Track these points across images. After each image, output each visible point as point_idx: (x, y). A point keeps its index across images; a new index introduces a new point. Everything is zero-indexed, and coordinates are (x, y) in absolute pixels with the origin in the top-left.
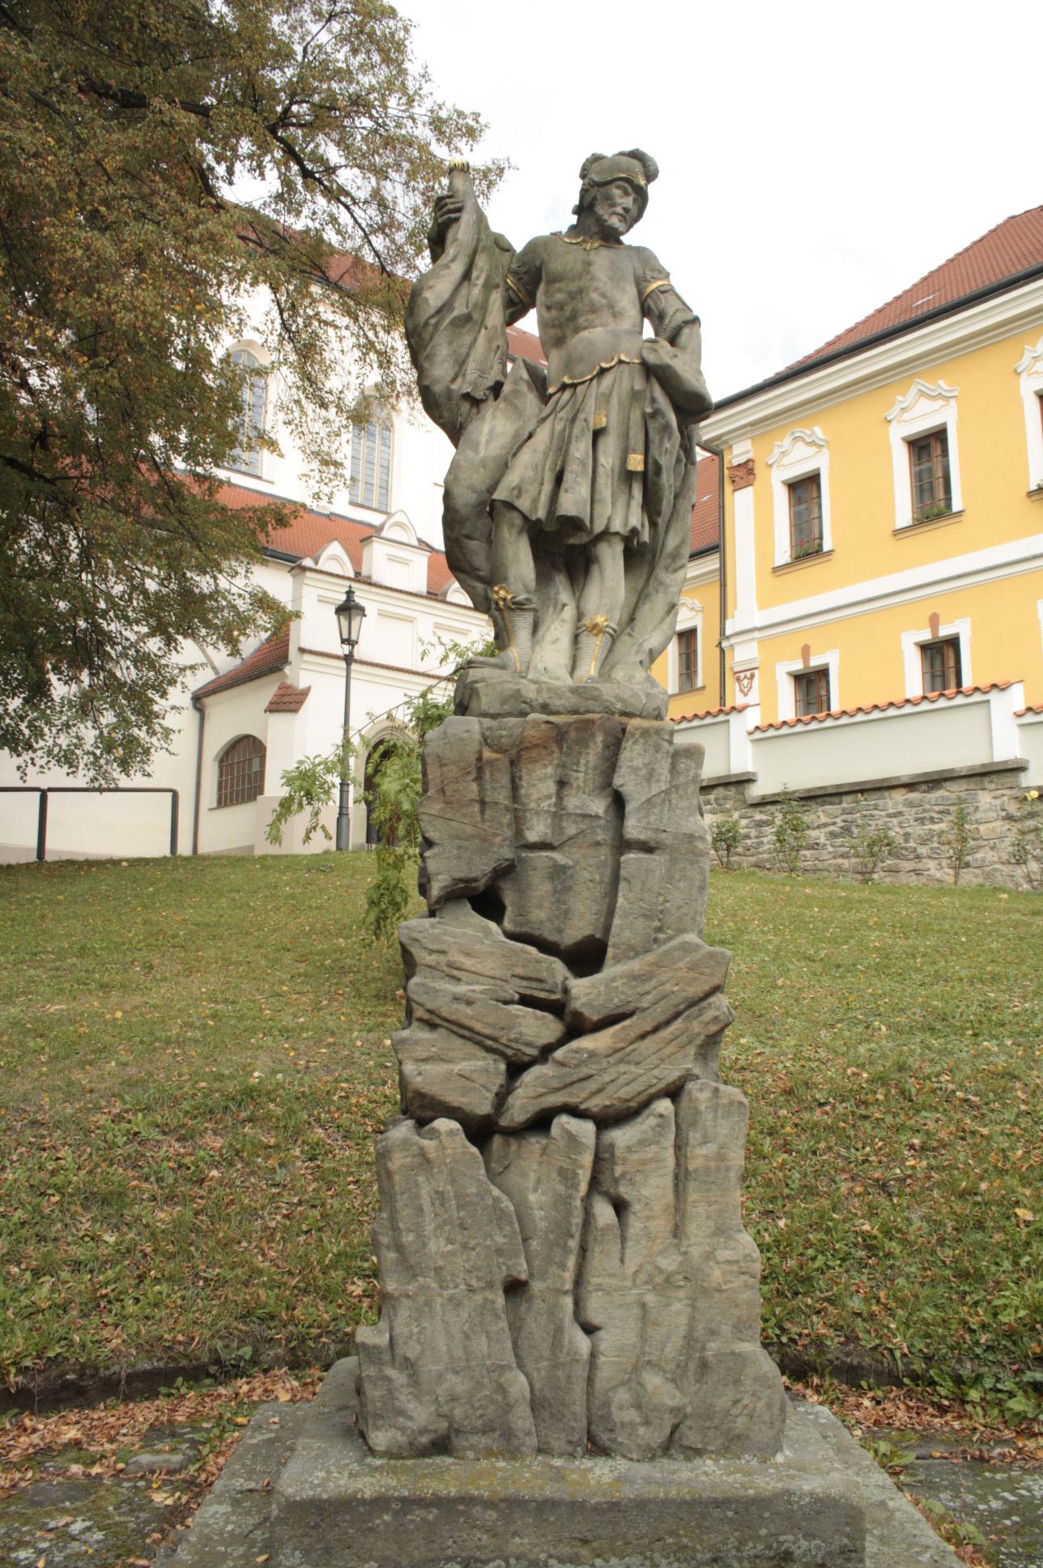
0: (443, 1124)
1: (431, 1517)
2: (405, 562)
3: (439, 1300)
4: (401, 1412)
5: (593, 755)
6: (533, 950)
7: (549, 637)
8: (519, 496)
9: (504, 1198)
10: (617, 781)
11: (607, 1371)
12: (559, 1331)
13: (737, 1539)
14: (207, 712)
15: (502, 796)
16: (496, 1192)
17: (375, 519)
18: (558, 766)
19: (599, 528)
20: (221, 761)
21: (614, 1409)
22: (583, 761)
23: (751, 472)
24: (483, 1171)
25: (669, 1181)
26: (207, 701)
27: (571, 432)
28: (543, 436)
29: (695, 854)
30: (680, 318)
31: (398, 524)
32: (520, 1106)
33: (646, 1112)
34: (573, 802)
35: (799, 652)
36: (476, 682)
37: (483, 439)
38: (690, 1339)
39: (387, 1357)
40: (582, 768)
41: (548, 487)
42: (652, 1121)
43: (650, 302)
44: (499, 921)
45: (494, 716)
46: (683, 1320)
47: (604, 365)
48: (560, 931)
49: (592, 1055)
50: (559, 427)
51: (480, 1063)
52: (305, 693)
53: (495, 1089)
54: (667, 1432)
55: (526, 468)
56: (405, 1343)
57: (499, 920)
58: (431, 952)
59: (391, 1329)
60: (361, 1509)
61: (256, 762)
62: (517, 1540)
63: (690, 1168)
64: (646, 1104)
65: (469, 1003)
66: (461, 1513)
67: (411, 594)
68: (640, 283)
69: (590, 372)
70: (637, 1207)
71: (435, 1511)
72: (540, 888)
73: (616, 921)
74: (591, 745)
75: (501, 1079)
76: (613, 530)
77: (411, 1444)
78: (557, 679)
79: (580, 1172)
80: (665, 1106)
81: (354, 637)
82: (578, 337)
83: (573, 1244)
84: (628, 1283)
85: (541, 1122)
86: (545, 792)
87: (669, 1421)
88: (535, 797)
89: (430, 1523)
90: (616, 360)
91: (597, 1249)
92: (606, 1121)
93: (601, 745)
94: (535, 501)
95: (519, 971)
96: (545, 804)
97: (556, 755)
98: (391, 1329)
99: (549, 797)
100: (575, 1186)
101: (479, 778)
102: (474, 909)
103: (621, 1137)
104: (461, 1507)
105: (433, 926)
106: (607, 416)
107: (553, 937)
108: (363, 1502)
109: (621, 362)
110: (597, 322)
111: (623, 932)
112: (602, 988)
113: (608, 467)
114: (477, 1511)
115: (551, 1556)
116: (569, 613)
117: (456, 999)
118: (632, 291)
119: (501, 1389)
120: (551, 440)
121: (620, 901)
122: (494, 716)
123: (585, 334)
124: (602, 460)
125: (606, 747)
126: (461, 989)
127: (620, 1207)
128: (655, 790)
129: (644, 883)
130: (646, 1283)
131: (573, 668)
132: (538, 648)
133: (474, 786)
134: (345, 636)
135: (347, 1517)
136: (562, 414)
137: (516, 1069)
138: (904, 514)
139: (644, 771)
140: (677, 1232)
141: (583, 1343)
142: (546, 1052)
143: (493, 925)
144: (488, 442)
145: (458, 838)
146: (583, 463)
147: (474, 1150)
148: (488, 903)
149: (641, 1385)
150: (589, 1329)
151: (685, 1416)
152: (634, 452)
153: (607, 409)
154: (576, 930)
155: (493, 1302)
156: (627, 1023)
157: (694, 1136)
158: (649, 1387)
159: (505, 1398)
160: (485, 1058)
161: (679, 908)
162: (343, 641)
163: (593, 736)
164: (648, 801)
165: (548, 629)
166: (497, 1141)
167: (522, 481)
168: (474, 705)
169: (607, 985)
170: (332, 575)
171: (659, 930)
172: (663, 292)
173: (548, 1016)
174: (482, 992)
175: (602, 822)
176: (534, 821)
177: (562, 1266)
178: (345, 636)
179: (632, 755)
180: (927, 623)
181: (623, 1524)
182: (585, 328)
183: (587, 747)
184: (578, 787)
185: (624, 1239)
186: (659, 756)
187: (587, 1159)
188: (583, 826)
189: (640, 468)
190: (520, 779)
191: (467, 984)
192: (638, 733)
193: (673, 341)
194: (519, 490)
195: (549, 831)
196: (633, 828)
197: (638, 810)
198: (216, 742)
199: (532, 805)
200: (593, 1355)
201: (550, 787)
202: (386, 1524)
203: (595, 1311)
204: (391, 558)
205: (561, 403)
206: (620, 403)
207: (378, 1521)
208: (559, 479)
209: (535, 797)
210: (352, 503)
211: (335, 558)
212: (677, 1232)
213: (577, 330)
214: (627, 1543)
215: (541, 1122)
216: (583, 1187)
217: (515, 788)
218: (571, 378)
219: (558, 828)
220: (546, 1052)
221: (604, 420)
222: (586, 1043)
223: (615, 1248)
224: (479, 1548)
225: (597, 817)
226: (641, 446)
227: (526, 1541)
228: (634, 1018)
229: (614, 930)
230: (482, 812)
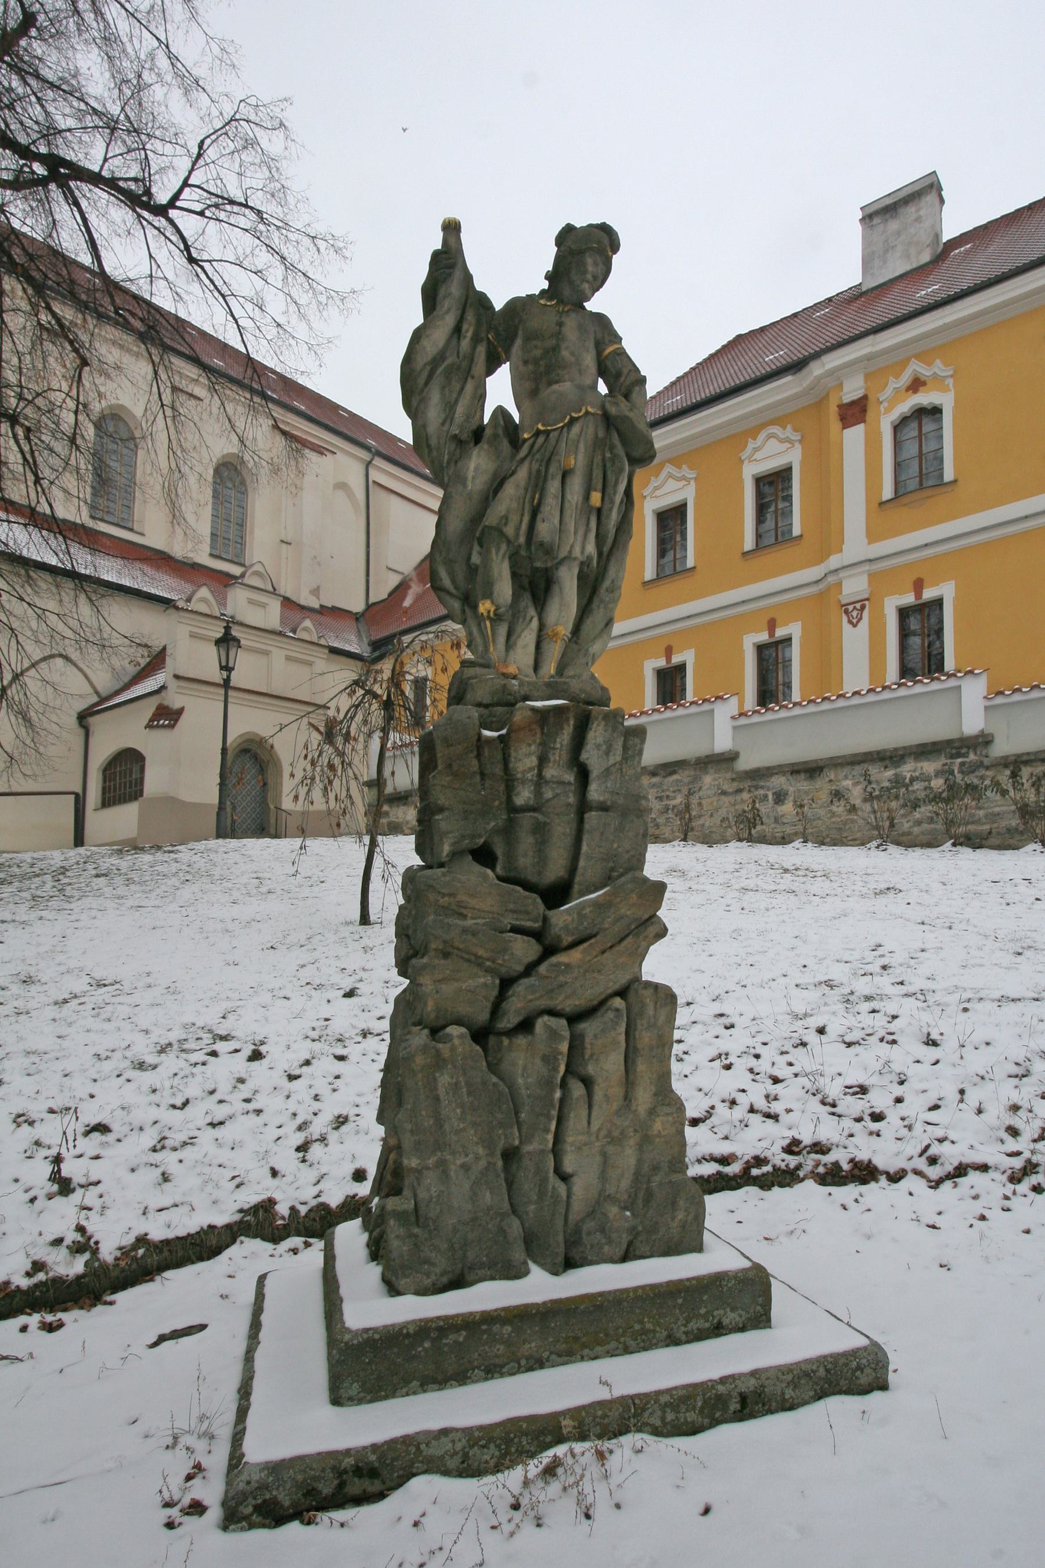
0: (454, 1030)
1: (461, 1339)
2: (263, 606)
3: (453, 1167)
4: (427, 1261)
5: (565, 737)
6: (518, 888)
7: (520, 643)
8: (506, 524)
9: (501, 1083)
10: (584, 756)
11: (578, 1207)
12: (544, 1180)
13: (685, 1319)
14: (91, 729)
15: (498, 770)
16: (495, 1079)
17: (236, 570)
18: (540, 744)
19: (563, 554)
20: (105, 770)
21: (584, 1235)
22: (558, 740)
23: (864, 411)
24: (484, 1063)
25: (622, 1058)
26: (92, 720)
27: (546, 471)
28: (522, 474)
29: (640, 811)
30: (632, 377)
31: (257, 573)
32: (511, 1016)
33: (605, 1008)
34: (550, 772)
35: (663, 651)
36: (469, 678)
37: (470, 474)
38: (637, 1175)
39: (413, 1219)
40: (558, 746)
41: (526, 519)
42: (611, 1015)
43: (609, 363)
44: (493, 869)
45: (486, 706)
46: (633, 1161)
47: (574, 415)
48: (540, 873)
49: (568, 966)
50: (535, 466)
51: (482, 980)
52: (180, 712)
53: (492, 999)
54: (624, 1246)
55: (511, 500)
56: (427, 1206)
57: (493, 868)
58: (444, 895)
59: (415, 1196)
60: (407, 1341)
61: (136, 768)
62: (527, 1346)
63: (639, 1046)
64: (602, 1003)
65: (474, 934)
66: (485, 1331)
67: (255, 628)
68: (599, 347)
69: (562, 420)
70: (600, 1080)
71: (464, 1333)
72: (526, 842)
73: (582, 863)
74: (566, 727)
75: (495, 993)
76: (573, 556)
77: (434, 1284)
78: (527, 676)
79: (560, 1057)
80: (618, 1002)
81: (231, 665)
82: (549, 390)
83: (554, 1113)
84: (593, 1138)
85: (526, 1026)
86: (529, 765)
87: (625, 1239)
88: (521, 769)
89: (460, 1344)
90: (583, 411)
91: (572, 1115)
92: (574, 1019)
93: (572, 727)
94: (518, 529)
95: (511, 906)
96: (529, 776)
97: (538, 735)
98: (415, 1196)
99: (531, 769)
100: (555, 1069)
101: (479, 756)
102: (474, 859)
103: (590, 1028)
104: (484, 1327)
105: (444, 875)
106: (575, 459)
107: (534, 879)
108: (408, 1335)
109: (587, 413)
110: (567, 377)
111: (588, 868)
112: (575, 916)
113: (574, 503)
114: (496, 1328)
115: (551, 1353)
116: (535, 624)
117: (465, 930)
118: (593, 352)
119: (502, 1231)
120: (530, 479)
121: (585, 848)
122: (486, 706)
123: (556, 387)
124: (568, 496)
125: (576, 728)
126: (469, 922)
127: (588, 1083)
128: (611, 761)
129: (602, 834)
130: (606, 1137)
131: (536, 667)
132: (511, 652)
133: (475, 762)
134: (224, 664)
135: (395, 1350)
136: (538, 456)
137: (506, 983)
138: (749, 543)
139: (604, 747)
140: (628, 1098)
141: (562, 1188)
142: (530, 969)
143: (489, 872)
144: (473, 478)
145: (464, 803)
146: (556, 497)
147: (478, 1048)
148: (484, 856)
149: (605, 1214)
150: (565, 1178)
151: (638, 1234)
152: (595, 490)
153: (576, 454)
154: (555, 871)
155: (495, 1164)
156: (593, 941)
157: (641, 1024)
158: (611, 1216)
159: (505, 1237)
160: (485, 977)
161: (628, 852)
162: (222, 668)
163: (567, 720)
164: (607, 769)
165: (519, 636)
166: (492, 1040)
167: (508, 511)
168: (469, 696)
169: (579, 913)
170: (201, 614)
171: (612, 869)
172: (619, 355)
173: (533, 941)
174: (484, 925)
175: (573, 788)
176: (520, 788)
177: (547, 1131)
178: (224, 664)
179: (596, 734)
180: (766, 626)
181: (604, 1321)
182: (557, 382)
183: (562, 729)
184: (555, 761)
185: (590, 1107)
186: (615, 735)
187: (564, 1047)
188: (558, 791)
189: (598, 504)
190: (509, 756)
191: (472, 918)
192: (600, 717)
193: (627, 396)
194: (505, 519)
195: (532, 796)
196: (595, 792)
197: (598, 777)
198: (100, 754)
199: (519, 776)
200: (569, 1196)
201: (533, 761)
202: (426, 1350)
203: (569, 1164)
204: (251, 602)
205: (536, 447)
206: (586, 449)
207: (420, 1349)
208: (535, 512)
209: (521, 769)
210: (211, 555)
211: (204, 600)
212: (628, 1098)
213: (550, 383)
214: (607, 1335)
215: (526, 1026)
216: (562, 1069)
217: (506, 761)
218: (543, 425)
219: (538, 793)
220: (530, 969)
221: (573, 462)
222: (562, 958)
223: (584, 1113)
224: (496, 1356)
225: (569, 783)
226: (600, 486)
227: (533, 1345)
228: (598, 937)
229: (580, 871)
230: (483, 779)
